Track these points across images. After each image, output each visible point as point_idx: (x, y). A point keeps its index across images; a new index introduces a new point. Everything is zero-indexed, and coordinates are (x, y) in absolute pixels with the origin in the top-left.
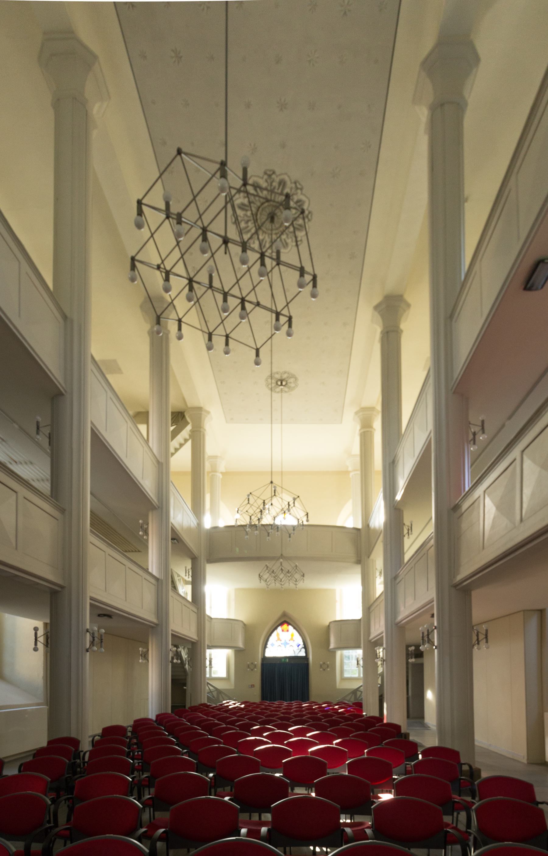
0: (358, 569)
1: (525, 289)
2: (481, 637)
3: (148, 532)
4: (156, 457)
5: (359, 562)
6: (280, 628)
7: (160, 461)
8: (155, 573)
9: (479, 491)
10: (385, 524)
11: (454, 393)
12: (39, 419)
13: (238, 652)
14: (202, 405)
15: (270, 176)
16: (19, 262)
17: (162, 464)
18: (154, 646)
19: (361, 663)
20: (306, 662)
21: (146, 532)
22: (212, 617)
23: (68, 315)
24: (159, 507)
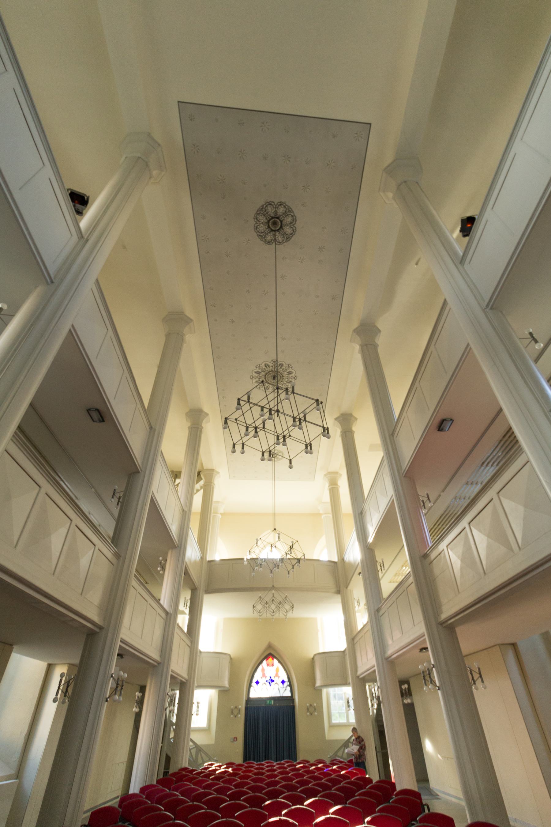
0: (338, 598)
1: (439, 430)
2: (476, 676)
3: (165, 567)
4: (182, 507)
5: (338, 592)
6: (265, 662)
7: (185, 510)
8: (166, 606)
9: (443, 546)
10: (362, 561)
11: (404, 477)
12: (116, 487)
13: (223, 693)
14: (214, 468)
15: (294, 378)
16: (137, 404)
17: (186, 512)
18: (152, 690)
19: (351, 703)
20: (292, 704)
21: (163, 568)
22: (202, 651)
23: (153, 427)
24: (178, 546)
